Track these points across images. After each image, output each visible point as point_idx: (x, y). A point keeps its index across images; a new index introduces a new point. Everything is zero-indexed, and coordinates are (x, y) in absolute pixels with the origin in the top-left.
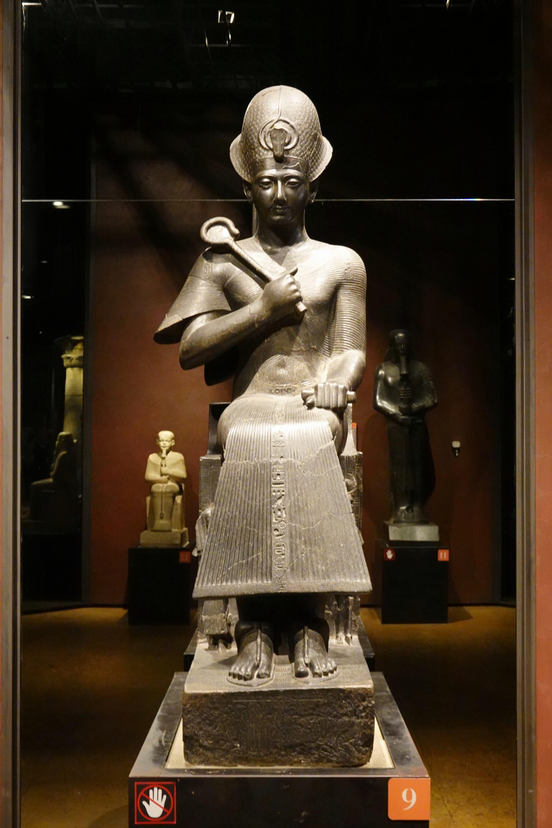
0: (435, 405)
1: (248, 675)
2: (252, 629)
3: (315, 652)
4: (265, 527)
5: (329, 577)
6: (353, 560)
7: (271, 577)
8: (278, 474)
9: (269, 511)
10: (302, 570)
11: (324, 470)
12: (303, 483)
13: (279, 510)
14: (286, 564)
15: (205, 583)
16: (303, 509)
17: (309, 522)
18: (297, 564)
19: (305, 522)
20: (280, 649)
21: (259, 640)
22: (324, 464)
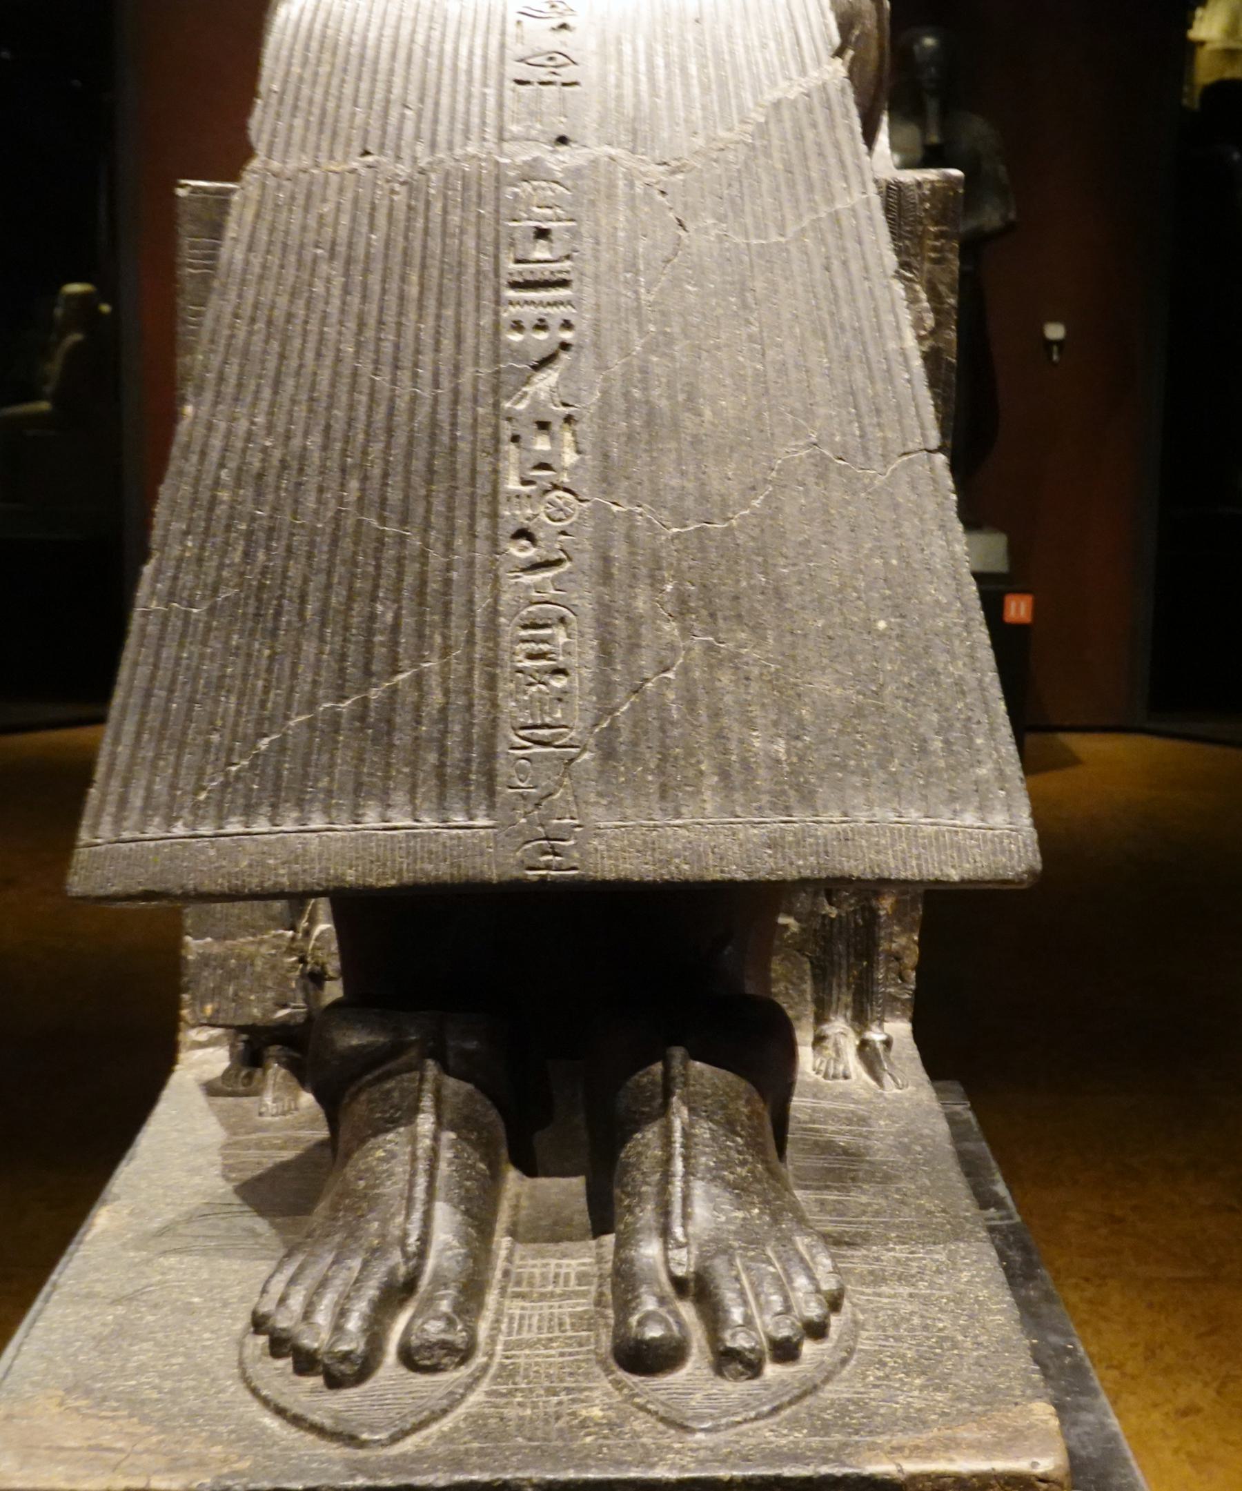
0: (1008, 228)
1: (346, 1357)
2: (396, 1050)
3: (725, 1199)
4: (461, 522)
5: (807, 798)
6: (941, 708)
7: (491, 792)
8: (542, 234)
9: (485, 432)
10: (664, 759)
11: (790, 217)
12: (676, 282)
13: (543, 426)
14: (576, 721)
15: (133, 817)
16: (676, 425)
17: (703, 498)
18: (637, 724)
19: (682, 495)
20: (542, 1140)
21: (425, 1123)
22: (792, 185)
